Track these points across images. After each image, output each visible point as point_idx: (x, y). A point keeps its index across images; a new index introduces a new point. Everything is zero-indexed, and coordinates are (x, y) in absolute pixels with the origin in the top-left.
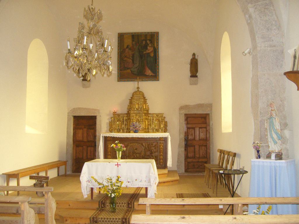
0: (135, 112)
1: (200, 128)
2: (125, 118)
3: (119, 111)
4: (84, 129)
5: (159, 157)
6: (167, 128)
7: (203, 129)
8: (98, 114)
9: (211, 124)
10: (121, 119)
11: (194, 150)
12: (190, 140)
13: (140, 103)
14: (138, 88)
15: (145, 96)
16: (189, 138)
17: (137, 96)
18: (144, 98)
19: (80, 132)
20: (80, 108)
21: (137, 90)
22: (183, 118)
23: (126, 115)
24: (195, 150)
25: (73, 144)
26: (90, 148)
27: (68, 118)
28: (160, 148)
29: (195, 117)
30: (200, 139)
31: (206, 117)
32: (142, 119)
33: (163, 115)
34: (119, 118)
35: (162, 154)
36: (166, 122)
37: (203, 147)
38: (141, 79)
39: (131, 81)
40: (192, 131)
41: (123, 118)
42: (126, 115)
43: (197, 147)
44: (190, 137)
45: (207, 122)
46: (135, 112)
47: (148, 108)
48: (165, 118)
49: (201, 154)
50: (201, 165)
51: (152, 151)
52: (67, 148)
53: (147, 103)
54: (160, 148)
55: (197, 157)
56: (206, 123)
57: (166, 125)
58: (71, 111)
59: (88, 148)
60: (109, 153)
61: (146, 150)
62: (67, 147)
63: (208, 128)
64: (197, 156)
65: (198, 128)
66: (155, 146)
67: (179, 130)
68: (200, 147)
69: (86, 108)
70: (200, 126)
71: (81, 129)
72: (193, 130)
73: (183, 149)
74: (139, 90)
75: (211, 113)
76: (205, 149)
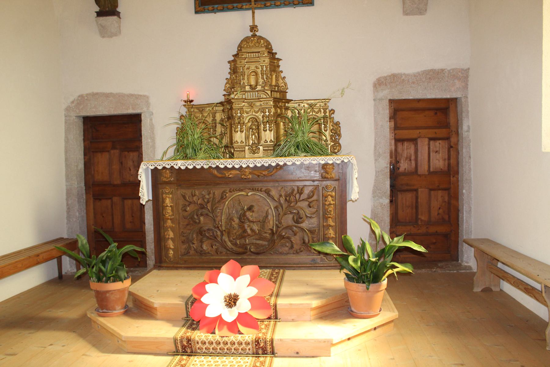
0: (248, 96)
1: (430, 139)
2: (218, 117)
3: (200, 98)
4: (112, 152)
5: (322, 233)
6: (340, 142)
7: (440, 141)
8: (145, 109)
9: (465, 128)
10: (210, 120)
11: (414, 201)
12: (405, 174)
13: (259, 71)
14: (253, 28)
15: (274, 51)
16: (402, 169)
17: (249, 50)
18: (272, 55)
19: (102, 160)
20: (97, 94)
21: (250, 34)
22: (386, 112)
23: (222, 108)
24: (417, 202)
25: (86, 193)
26: (130, 202)
27: (66, 123)
28: (324, 205)
29: (415, 110)
30: (431, 170)
31: (449, 107)
32: (268, 117)
33: (328, 104)
34: (203, 116)
35: (331, 222)
36: (338, 124)
37: (440, 193)
38: (263, 3)
39: (233, 9)
40: (407, 149)
41: (214, 117)
42: (222, 108)
43: (423, 194)
44: (404, 166)
45: (452, 120)
46: (248, 96)
47: (286, 84)
48: (333, 111)
49: (434, 213)
50: (434, 243)
51: (301, 212)
52: (68, 205)
53: (282, 72)
54: (324, 205)
55: (422, 220)
56: (447, 126)
57: (336, 133)
58: (73, 105)
59: (126, 201)
60: (169, 221)
61: (280, 210)
62: (70, 202)
63: (453, 140)
64: (423, 217)
65: (427, 140)
66: (309, 198)
67: (375, 147)
68: (432, 192)
69: (111, 93)
70: (431, 133)
71: (103, 151)
72: (413, 147)
73: (386, 201)
74: (257, 33)
75: (466, 97)
76: (446, 199)
